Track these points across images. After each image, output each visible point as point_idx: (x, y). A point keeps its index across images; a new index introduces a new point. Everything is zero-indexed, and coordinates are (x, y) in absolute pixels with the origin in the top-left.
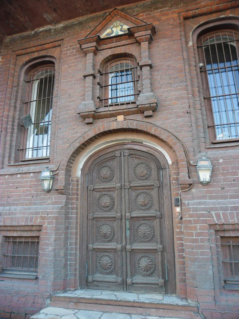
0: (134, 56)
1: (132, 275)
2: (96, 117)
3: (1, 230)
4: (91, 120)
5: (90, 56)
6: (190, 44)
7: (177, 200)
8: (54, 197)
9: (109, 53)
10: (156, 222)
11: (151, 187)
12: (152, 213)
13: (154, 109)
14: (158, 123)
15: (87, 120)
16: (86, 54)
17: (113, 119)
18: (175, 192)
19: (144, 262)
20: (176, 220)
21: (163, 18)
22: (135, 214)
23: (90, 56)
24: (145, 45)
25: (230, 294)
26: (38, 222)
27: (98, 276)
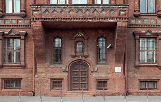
0: (62, 27)
1: (81, 88)
2: (75, 56)
3: (116, 1)
4: (74, 57)
5: (73, 40)
6: (96, 41)
7: (90, 74)
8: (65, 73)
9: (77, 40)
10: (86, 78)
11: (85, 71)
12: (85, 76)
13: (87, 56)
14: (88, 59)
15: (73, 57)
16: (72, 40)
17: (79, 57)
18: (90, 72)
19: (83, 85)
20: (90, 78)
21: (90, 33)
22: (82, 70)
23: (73, 40)
24: (86, 40)
25: (77, 21)
26: (63, 78)
27: (74, 88)
